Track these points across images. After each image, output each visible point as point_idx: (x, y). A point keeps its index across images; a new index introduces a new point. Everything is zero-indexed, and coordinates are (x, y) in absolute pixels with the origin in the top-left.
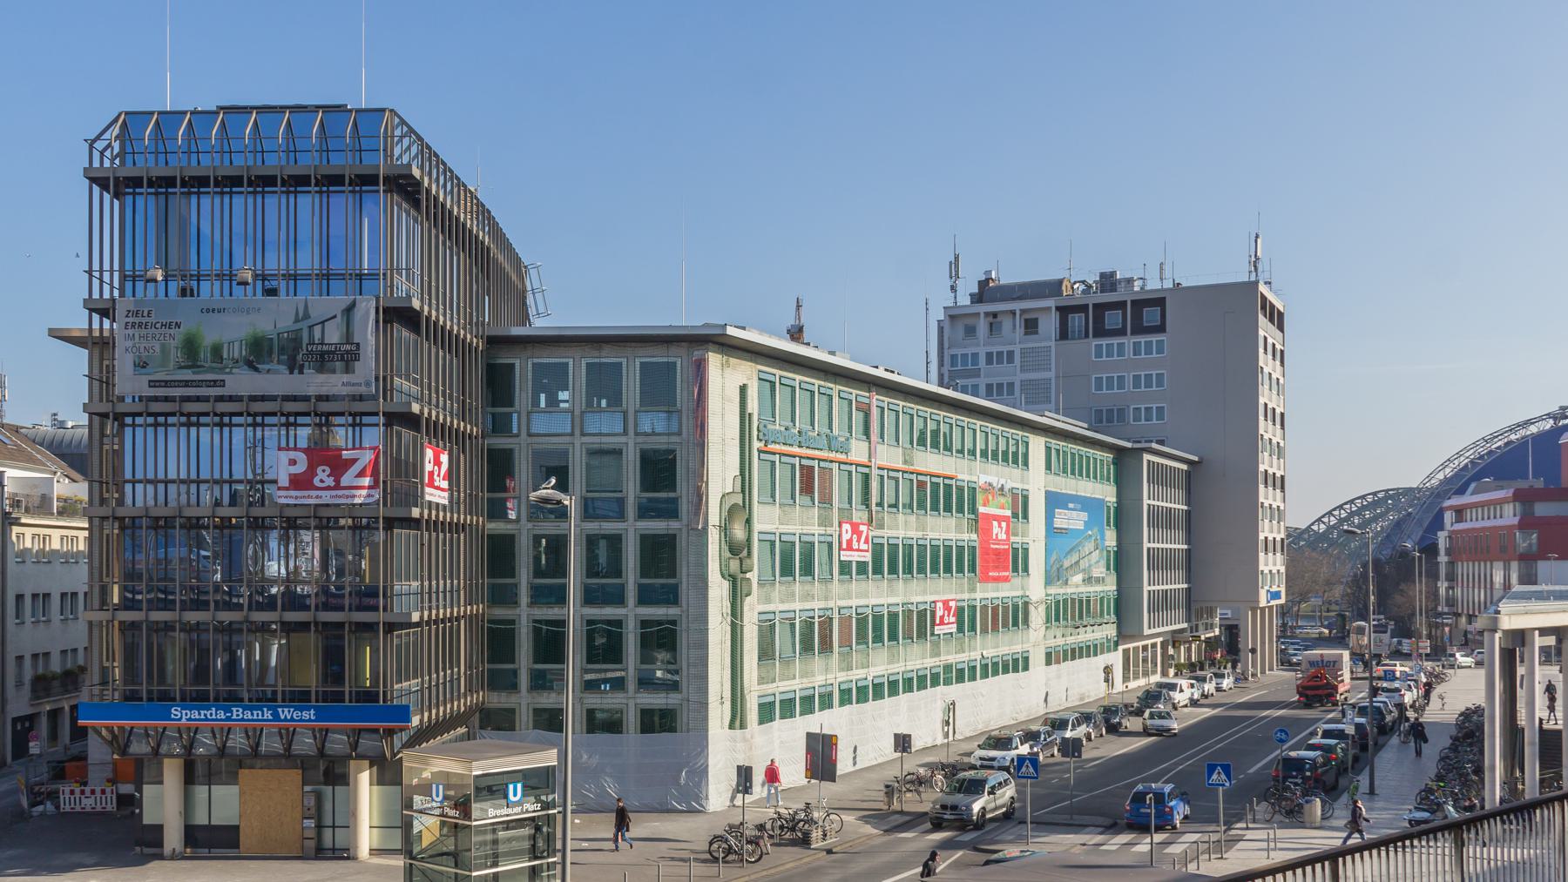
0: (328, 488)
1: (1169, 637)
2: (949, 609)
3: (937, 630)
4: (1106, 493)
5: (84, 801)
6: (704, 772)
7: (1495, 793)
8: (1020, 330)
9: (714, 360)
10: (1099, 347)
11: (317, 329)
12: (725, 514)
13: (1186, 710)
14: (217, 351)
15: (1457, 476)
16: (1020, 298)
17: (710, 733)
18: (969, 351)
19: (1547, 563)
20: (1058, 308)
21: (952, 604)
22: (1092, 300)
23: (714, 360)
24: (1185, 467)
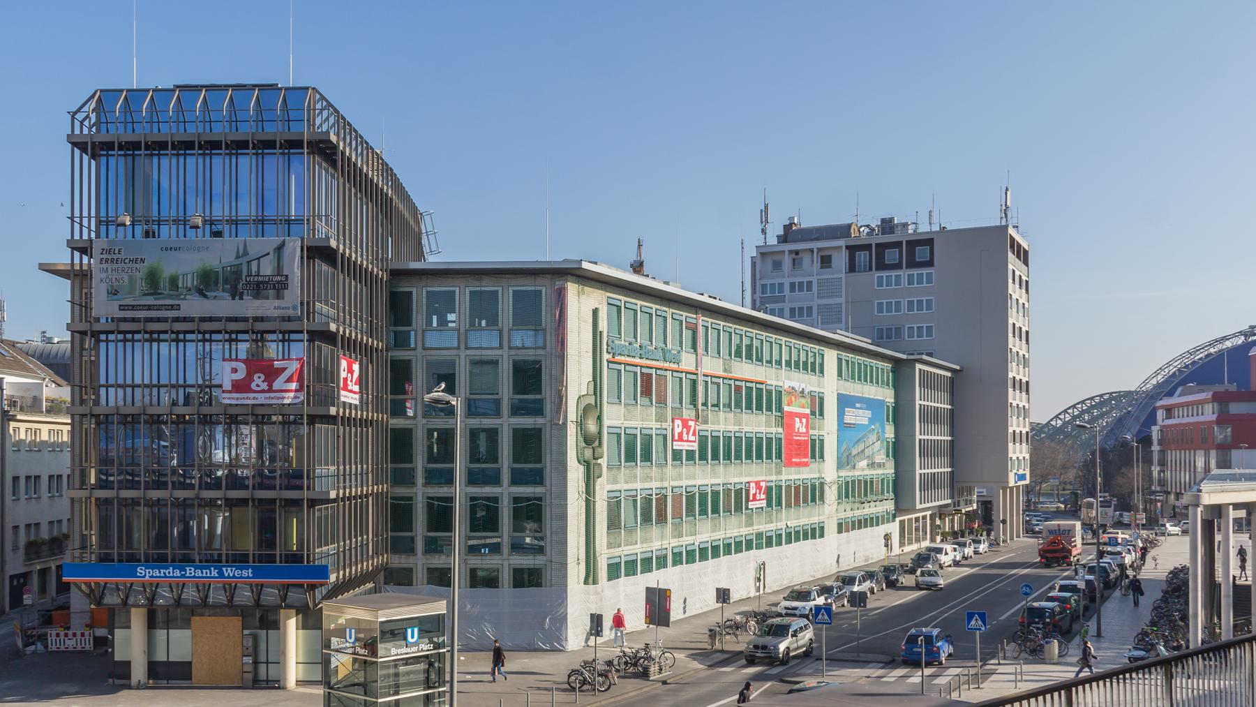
0: (263, 391)
1: (936, 511)
2: (760, 488)
3: (751, 505)
4: (886, 395)
5: (68, 642)
6: (564, 618)
7: (1197, 635)
8: (817, 265)
9: (572, 289)
10: (880, 278)
11: (254, 264)
12: (581, 412)
13: (950, 569)
14: (173, 281)
15: (1167, 381)
16: (817, 239)
17: (569, 587)
18: (776, 281)
19: (1240, 451)
20: (847, 247)
21: (763, 484)
22: (874, 240)
23: (572, 289)
24: (949, 374)
